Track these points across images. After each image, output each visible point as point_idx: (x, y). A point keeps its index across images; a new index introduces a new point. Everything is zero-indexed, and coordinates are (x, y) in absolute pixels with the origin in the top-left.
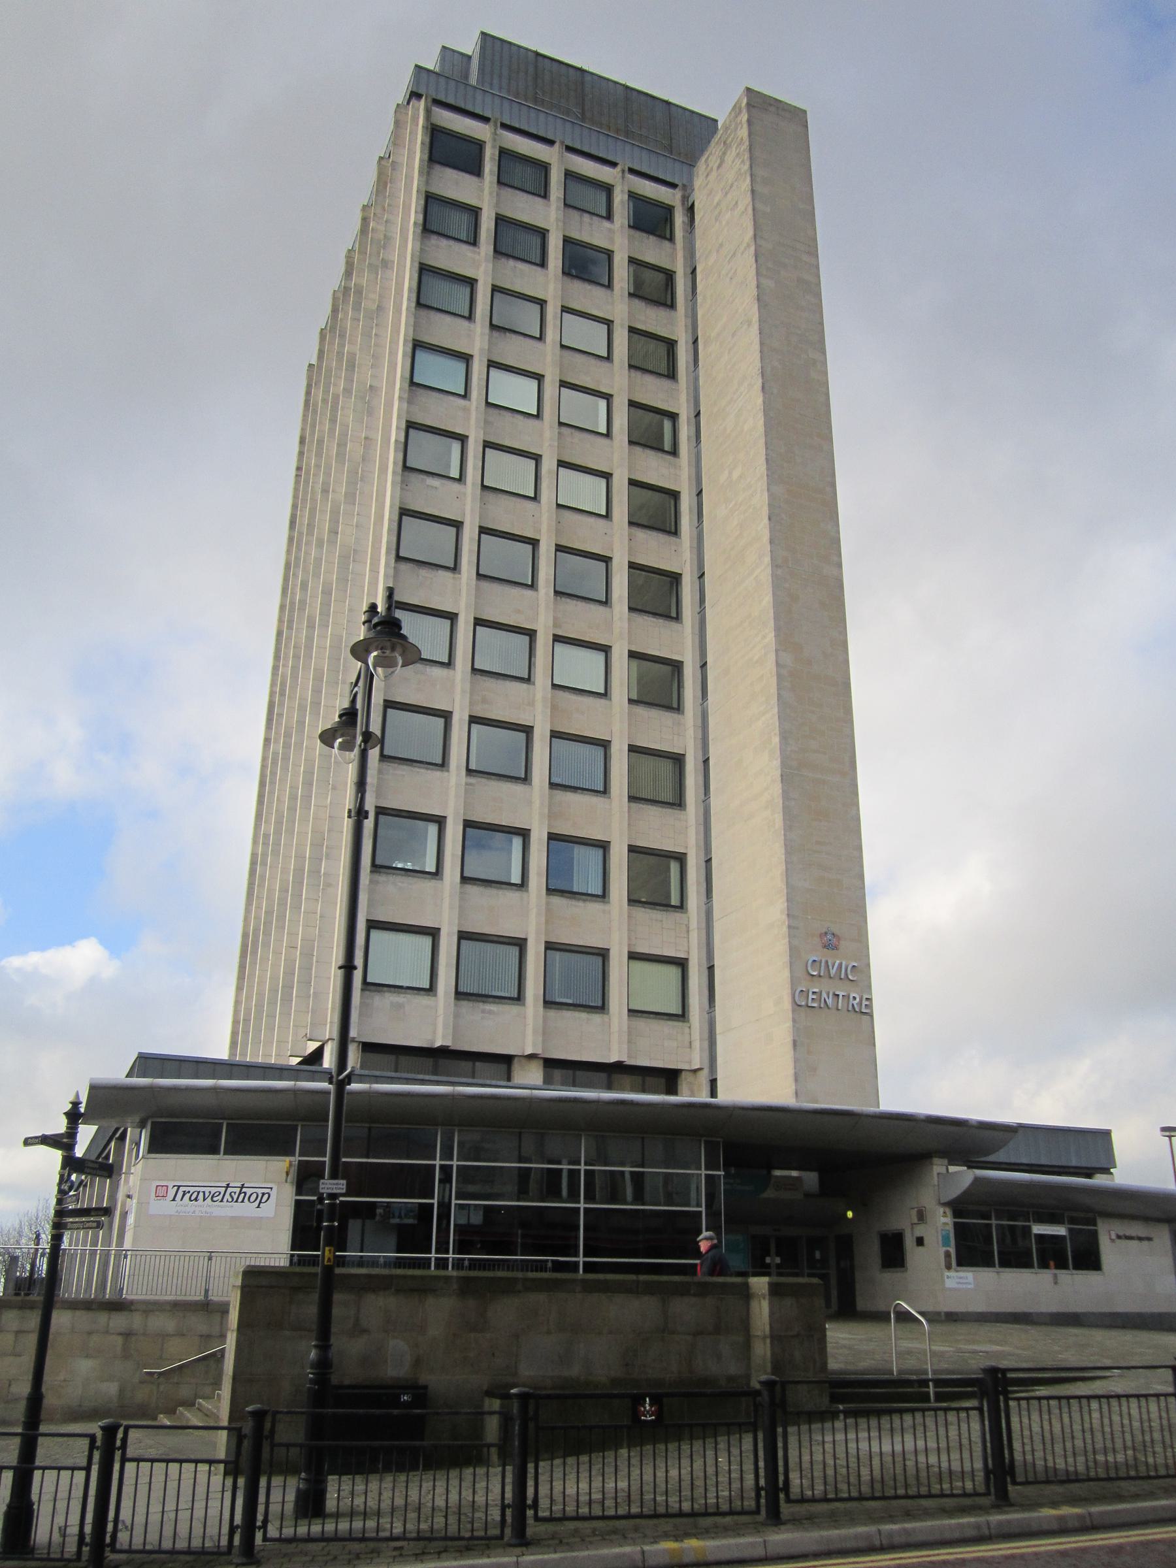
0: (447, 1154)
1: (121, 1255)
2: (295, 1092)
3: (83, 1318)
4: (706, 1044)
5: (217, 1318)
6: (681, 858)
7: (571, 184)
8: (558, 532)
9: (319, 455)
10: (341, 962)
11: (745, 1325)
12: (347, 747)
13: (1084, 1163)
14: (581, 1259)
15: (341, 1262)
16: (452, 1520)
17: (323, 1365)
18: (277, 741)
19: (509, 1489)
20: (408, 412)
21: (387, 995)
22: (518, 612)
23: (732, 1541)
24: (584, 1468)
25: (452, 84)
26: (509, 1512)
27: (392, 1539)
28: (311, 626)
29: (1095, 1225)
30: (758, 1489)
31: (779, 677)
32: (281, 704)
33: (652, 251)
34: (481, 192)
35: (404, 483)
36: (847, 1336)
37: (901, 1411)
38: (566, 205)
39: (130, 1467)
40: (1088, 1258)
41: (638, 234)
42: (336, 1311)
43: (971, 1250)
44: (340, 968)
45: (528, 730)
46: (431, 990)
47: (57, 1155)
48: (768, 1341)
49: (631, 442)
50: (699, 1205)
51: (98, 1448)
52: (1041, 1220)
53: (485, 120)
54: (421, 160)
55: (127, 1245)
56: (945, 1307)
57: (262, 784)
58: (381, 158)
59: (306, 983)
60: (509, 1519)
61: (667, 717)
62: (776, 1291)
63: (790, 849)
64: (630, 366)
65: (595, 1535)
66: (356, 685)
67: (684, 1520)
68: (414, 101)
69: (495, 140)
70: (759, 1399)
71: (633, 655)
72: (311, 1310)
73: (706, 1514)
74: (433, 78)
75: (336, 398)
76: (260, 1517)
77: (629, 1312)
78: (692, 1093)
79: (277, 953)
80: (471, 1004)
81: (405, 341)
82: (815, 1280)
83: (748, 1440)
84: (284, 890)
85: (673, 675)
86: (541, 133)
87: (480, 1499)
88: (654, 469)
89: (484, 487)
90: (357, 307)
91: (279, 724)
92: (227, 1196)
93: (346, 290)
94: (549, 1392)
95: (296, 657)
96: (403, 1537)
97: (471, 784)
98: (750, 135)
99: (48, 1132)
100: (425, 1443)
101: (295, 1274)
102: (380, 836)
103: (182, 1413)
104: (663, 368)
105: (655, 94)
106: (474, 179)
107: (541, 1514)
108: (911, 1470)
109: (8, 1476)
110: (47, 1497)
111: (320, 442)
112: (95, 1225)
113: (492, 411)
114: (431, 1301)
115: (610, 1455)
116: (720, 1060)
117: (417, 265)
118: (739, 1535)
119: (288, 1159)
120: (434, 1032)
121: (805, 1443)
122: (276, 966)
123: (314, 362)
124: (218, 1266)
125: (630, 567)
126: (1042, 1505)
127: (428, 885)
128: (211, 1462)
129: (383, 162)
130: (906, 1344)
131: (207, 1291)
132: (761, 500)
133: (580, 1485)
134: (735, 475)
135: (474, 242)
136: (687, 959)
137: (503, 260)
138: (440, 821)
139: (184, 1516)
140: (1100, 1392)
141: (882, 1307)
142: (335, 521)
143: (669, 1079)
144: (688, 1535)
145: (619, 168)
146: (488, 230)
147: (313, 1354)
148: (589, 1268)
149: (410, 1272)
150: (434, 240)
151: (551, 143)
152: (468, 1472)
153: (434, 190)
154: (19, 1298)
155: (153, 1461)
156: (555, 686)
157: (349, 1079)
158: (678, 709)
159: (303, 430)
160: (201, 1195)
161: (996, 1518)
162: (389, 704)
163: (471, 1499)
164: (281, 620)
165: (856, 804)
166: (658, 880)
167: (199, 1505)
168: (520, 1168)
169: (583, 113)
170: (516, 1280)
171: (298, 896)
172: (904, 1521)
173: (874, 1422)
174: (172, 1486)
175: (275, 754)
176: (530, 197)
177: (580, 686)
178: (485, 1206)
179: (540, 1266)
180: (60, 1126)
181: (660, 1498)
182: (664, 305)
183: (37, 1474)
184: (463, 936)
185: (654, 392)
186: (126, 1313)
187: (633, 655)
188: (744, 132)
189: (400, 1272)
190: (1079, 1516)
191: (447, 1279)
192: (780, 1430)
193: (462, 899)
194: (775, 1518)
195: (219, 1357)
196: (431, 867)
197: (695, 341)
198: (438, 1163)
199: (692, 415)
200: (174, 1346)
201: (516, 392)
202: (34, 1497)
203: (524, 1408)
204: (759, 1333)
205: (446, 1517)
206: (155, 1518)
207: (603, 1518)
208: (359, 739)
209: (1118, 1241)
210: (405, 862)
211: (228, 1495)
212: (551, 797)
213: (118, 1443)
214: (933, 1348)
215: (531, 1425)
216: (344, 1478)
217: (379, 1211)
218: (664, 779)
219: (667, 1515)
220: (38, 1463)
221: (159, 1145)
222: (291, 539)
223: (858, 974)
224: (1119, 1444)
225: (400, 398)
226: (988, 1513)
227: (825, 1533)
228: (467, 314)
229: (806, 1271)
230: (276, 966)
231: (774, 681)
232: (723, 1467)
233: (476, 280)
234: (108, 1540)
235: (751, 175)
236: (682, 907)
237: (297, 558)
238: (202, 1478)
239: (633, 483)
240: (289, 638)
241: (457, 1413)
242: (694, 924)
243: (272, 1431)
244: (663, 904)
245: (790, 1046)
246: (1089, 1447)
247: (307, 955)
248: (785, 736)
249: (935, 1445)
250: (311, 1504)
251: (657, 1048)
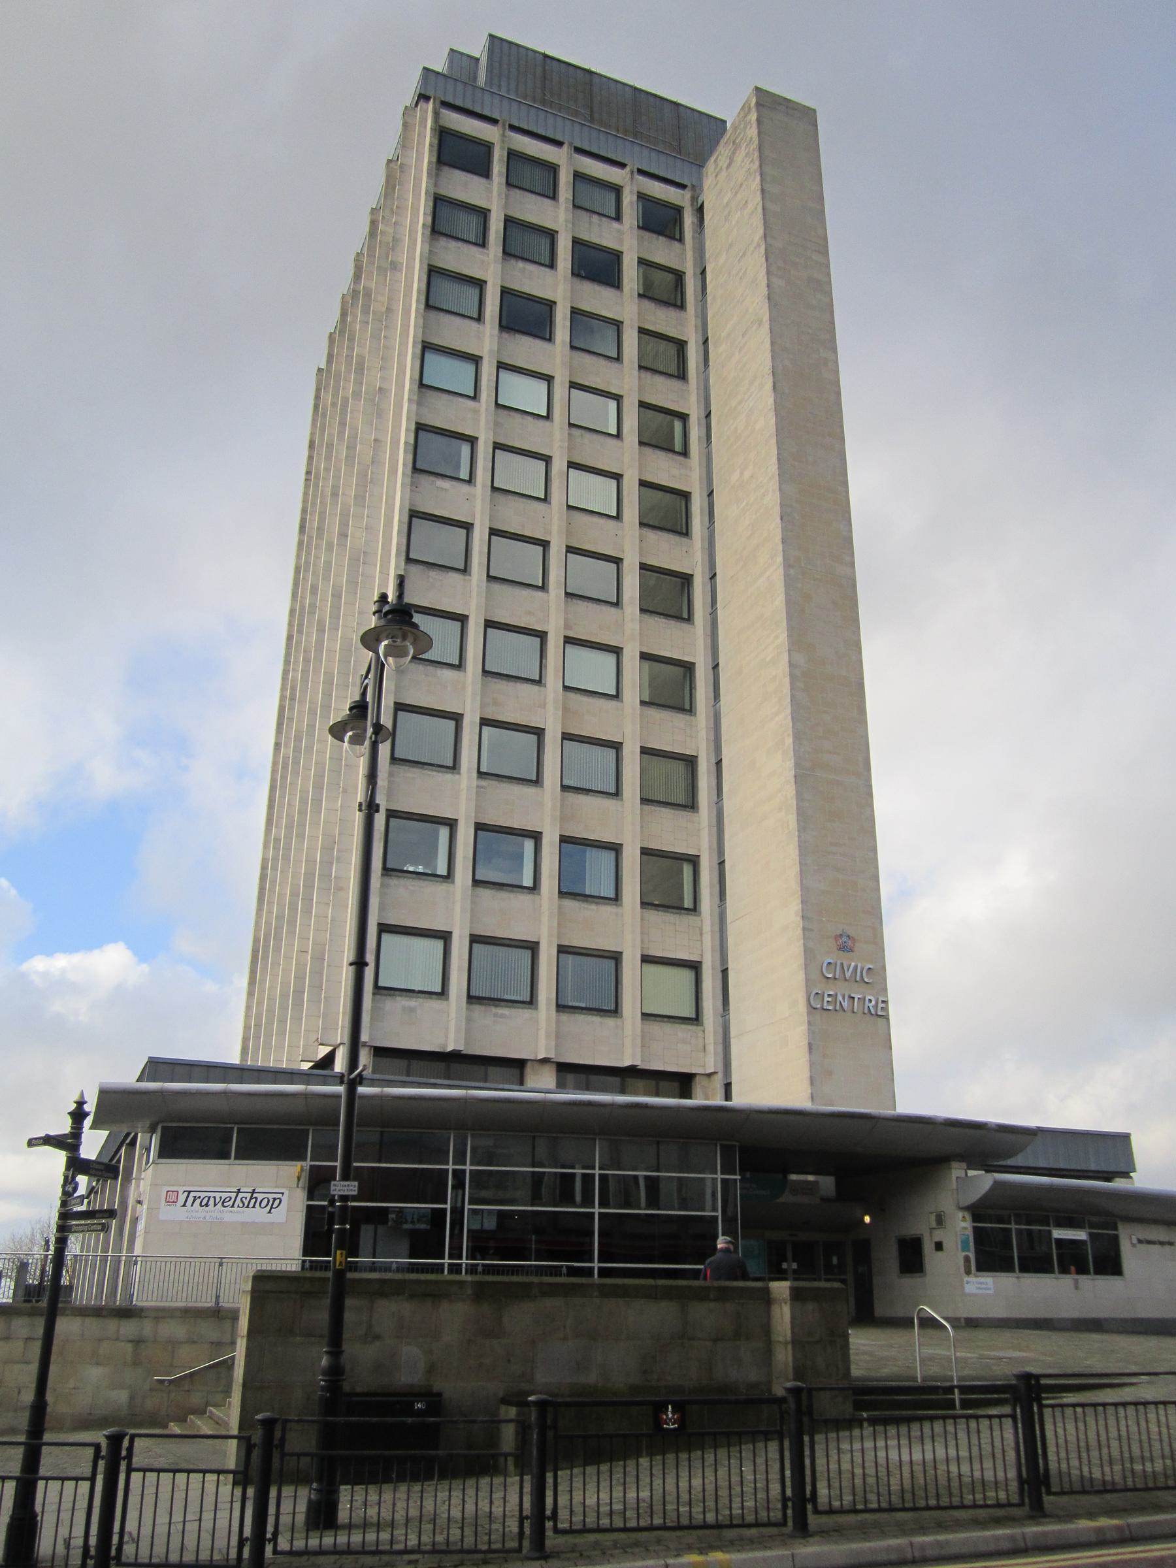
0: (460, 1158)
1: (132, 1261)
2: (306, 1096)
3: (93, 1325)
4: (720, 1048)
5: (228, 1324)
6: (694, 861)
7: (581, 186)
8: (569, 533)
9: (328, 458)
10: (352, 958)
11: (766, 1330)
12: (357, 740)
13: (1103, 1167)
14: (596, 1265)
15: (354, 1267)
16: (469, 1531)
17: (335, 1372)
18: (287, 745)
19: (527, 1500)
20: (417, 414)
21: (398, 998)
22: (529, 613)
23: (759, 1554)
24: (605, 1476)
25: (460, 86)
26: (527, 1524)
27: (406, 1552)
28: (321, 630)
29: (1116, 1229)
30: (784, 1500)
31: (792, 677)
32: (292, 708)
33: (662, 252)
34: (489, 194)
35: (414, 485)
36: (867, 1342)
37: (932, 1419)
38: (574, 206)
39: (136, 1477)
40: (1109, 1263)
41: (647, 234)
42: (348, 1316)
43: (991, 1255)
44: (351, 964)
45: (539, 733)
46: (443, 994)
47: (60, 1158)
48: (790, 1347)
49: (641, 443)
50: (714, 1209)
51: (103, 1458)
52: (1060, 1224)
53: (494, 121)
54: (430, 162)
55: (138, 1250)
56: (964, 1313)
57: (273, 788)
58: (389, 161)
59: (317, 986)
60: (527, 1531)
61: (679, 719)
62: (797, 1296)
64: (641, 367)
65: (615, 1547)
66: (366, 677)
67: (707, 1532)
68: (422, 104)
69: (503, 141)
70: (784, 1406)
71: (644, 656)
72: (321, 1316)
73: (732, 1526)
74: (441, 78)
75: (345, 400)
76: (270, 1528)
77: (647, 1317)
78: (705, 1097)
79: (288, 958)
80: (483, 1008)
81: (414, 342)
82: (836, 1285)
83: (773, 1446)
84: (294, 894)
85: (685, 677)
86: (550, 135)
87: (498, 1510)
88: (665, 470)
89: (494, 489)
90: (366, 311)
91: (290, 727)
92: (238, 1201)
93: (355, 293)
94: (568, 1399)
95: (306, 661)
96: (418, 1550)
97: (482, 787)
98: (759, 133)
99: (52, 1133)
100: (440, 1452)
101: (305, 1278)
102: (394, 840)
103: (193, 1422)
104: (673, 369)
105: (665, 96)
106: (483, 180)
107: (560, 1526)
108: (943, 1481)
109: (10, 1488)
110: (51, 1507)
111: (330, 446)
112: (100, 1227)
113: (500, 411)
114: (445, 1305)
115: (631, 1464)
116: (734, 1064)
117: (426, 267)
118: (766, 1548)
119: (299, 1164)
120: (447, 1037)
121: (833, 1453)
122: (286, 971)
123: (323, 366)
124: (229, 1274)
125: (641, 568)
126: (1077, 1516)
127: (441, 888)
128: (219, 1472)
129: (392, 165)
130: (928, 1351)
131: (218, 1297)
132: (772, 499)
133: (614, 1494)
134: (747, 475)
135: (483, 244)
136: (700, 963)
137: (513, 261)
138: (452, 824)
139: (192, 1527)
140: (1129, 1399)
141: (901, 1313)
142: (344, 524)
143: (684, 1082)
144: (712, 1548)
145: (628, 169)
146: (497, 232)
147: (325, 1361)
148: (603, 1272)
149: (423, 1277)
150: (443, 242)
151: (559, 144)
152: (485, 1481)
153: (443, 192)
154: (28, 1305)
155: (159, 1471)
156: (566, 688)
157: (360, 1080)
158: (690, 710)
159: (312, 434)
160: (212, 1200)
161: (1032, 1530)
162: (399, 707)
163: (487, 1510)
164: (291, 625)
165: (871, 806)
166: (672, 882)
167: (208, 1516)
168: (533, 1172)
169: (591, 115)
170: (530, 1284)
171: (308, 899)
172: (937, 1533)
173: (904, 1429)
174: (179, 1496)
175: (286, 758)
176: (539, 198)
177: (591, 692)
179: (556, 1271)
180: (64, 1126)
181: (684, 1509)
182: (674, 305)
183: (41, 1484)
184: (475, 939)
185: (664, 393)
187: (644, 656)
188: (753, 132)
189: (414, 1276)
190: (1118, 1528)
191: (461, 1284)
192: (806, 1438)
193: (473, 902)
194: (802, 1530)
195: (229, 1365)
196: (442, 870)
197: (706, 342)
198: (451, 1167)
199: (703, 415)
200: (184, 1352)
201: (526, 394)
202: (38, 1508)
203: (542, 1416)
204: (781, 1339)
205: (462, 1528)
206: (162, 1529)
207: (625, 1530)
208: (370, 731)
209: (1139, 1246)
210: (416, 864)
211: (237, 1506)
212: (563, 800)
213: (124, 1453)
214: (958, 1354)
215: (550, 1434)
216: (357, 1488)
217: (392, 1216)
218: (677, 781)
219: (691, 1527)
220: (42, 1471)
221: (169, 1150)
222: (300, 544)
223: (873, 976)
224: (1157, 1452)
225: (410, 400)
226: (1023, 1525)
227: (855, 1546)
228: (476, 316)
229: (823, 1277)
230: (286, 971)
231: (787, 680)
232: (749, 1476)
233: (485, 282)
234: (113, 1553)
235: (761, 175)
236: (695, 909)
237: (307, 563)
238: (210, 1487)
239: (643, 484)
240: (299, 642)
241: (474, 1422)
242: (707, 928)
243: (283, 1440)
244: (677, 907)
245: (806, 1049)
246: (1126, 1455)
247: (319, 958)
248: (797, 737)
249: (967, 1454)
250: (323, 1515)
251: (671, 1052)
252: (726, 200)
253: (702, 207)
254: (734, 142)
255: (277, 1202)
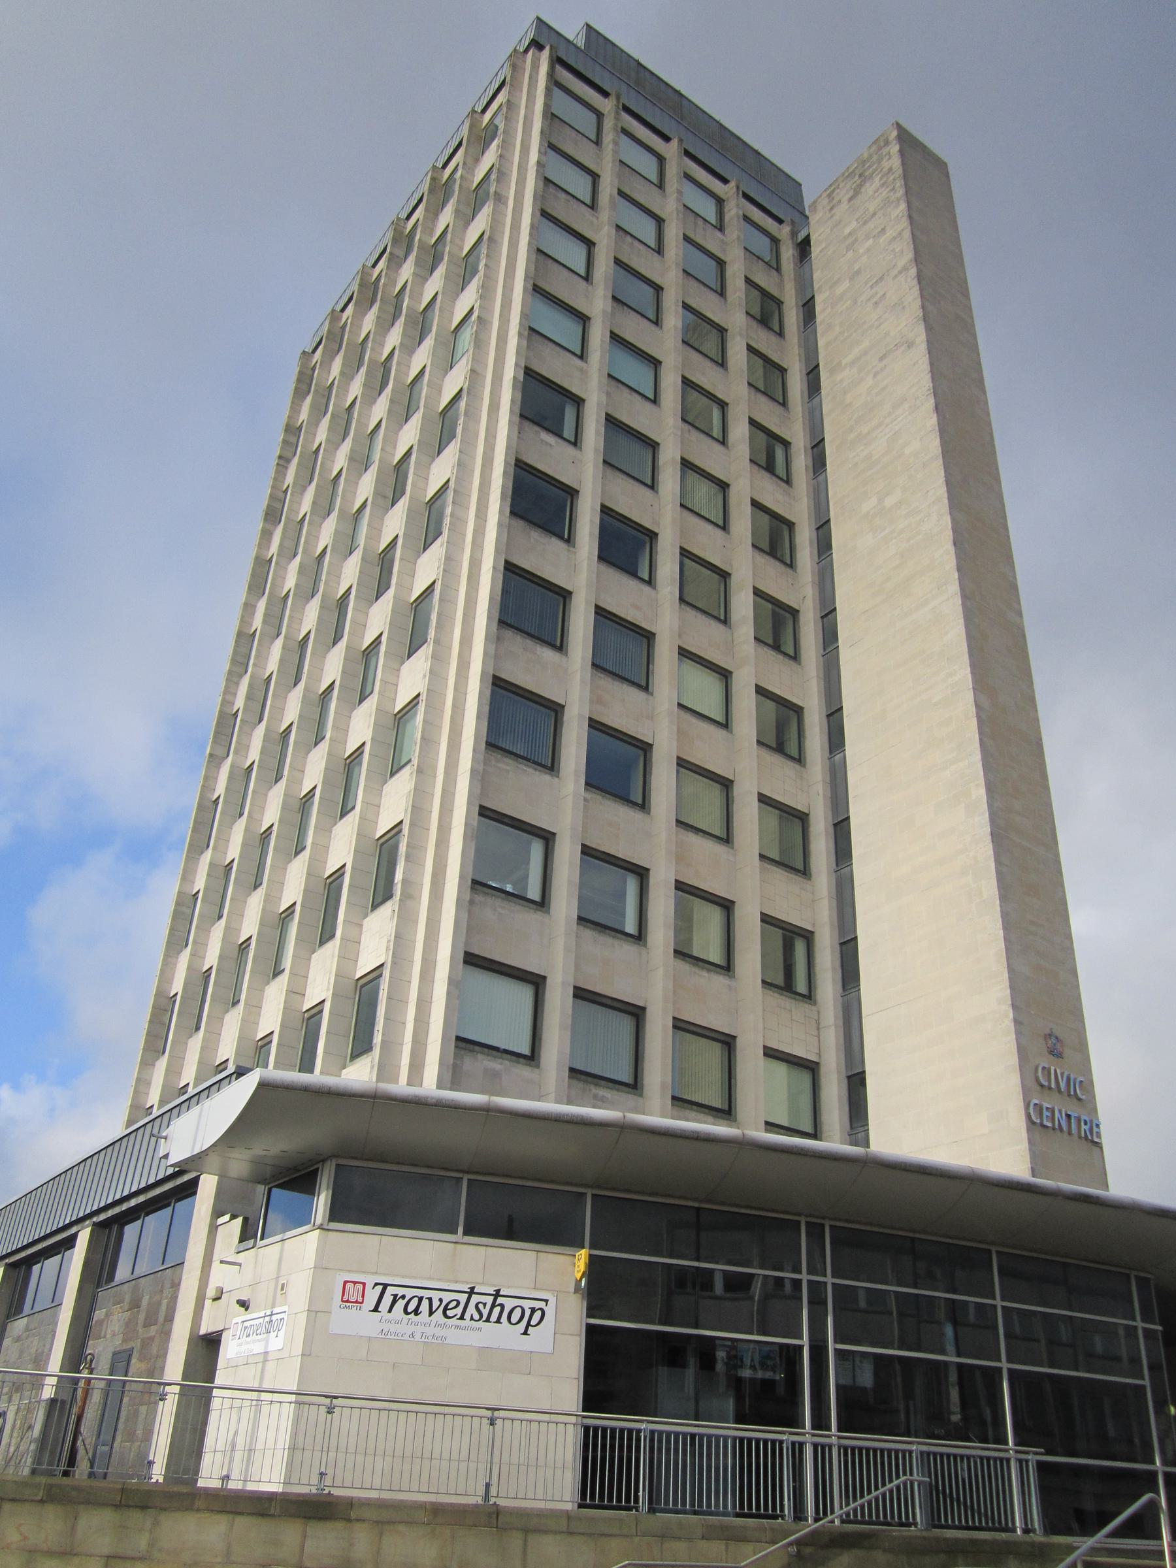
21: (480, 1056)
63: (1008, 925)
92: (471, 1309)
127: (533, 917)
160: (425, 1303)
178: (875, 1355)
186: (340, 1525)
252: (847, 231)
253: (806, 242)
254: (860, 176)
255: (538, 1314)
